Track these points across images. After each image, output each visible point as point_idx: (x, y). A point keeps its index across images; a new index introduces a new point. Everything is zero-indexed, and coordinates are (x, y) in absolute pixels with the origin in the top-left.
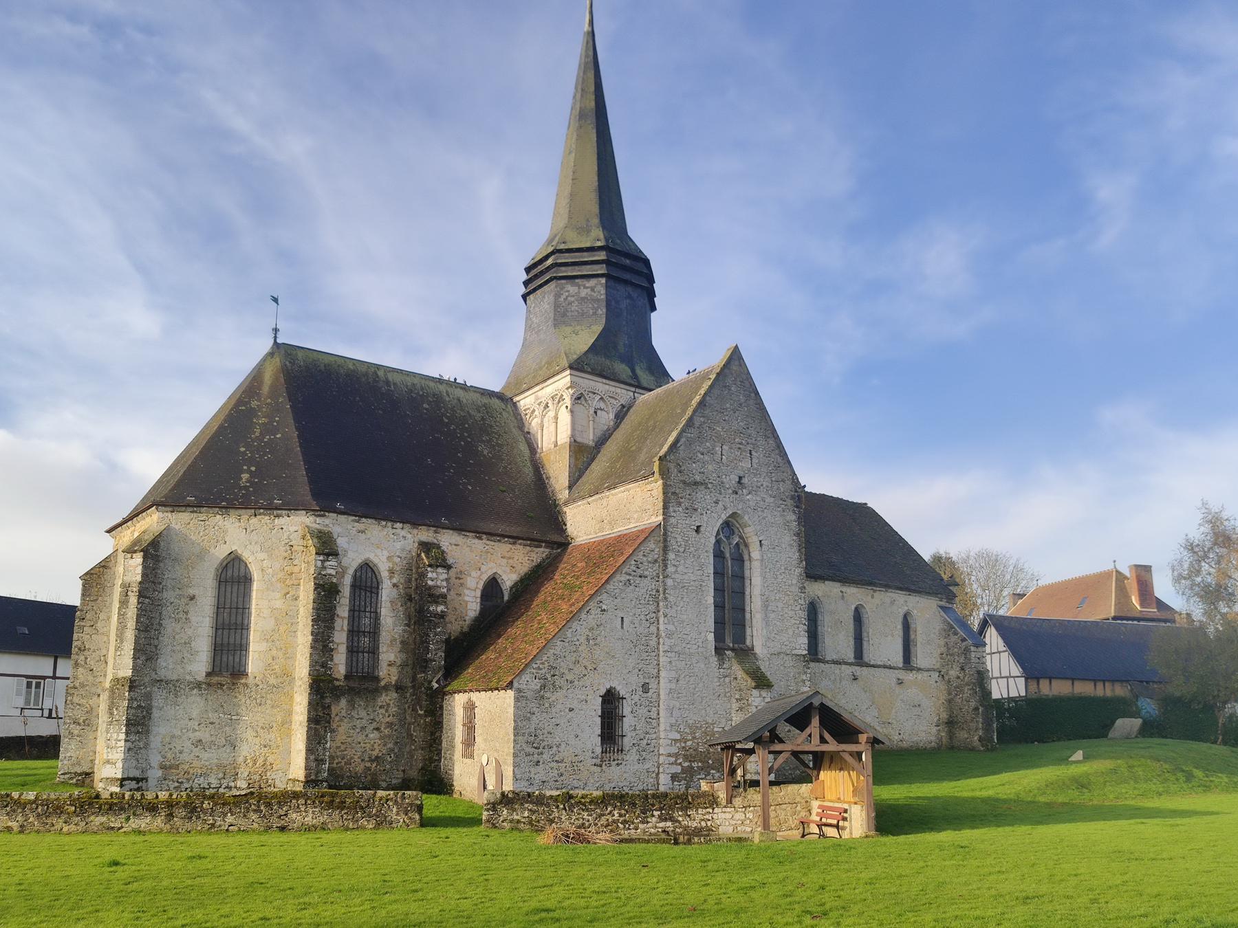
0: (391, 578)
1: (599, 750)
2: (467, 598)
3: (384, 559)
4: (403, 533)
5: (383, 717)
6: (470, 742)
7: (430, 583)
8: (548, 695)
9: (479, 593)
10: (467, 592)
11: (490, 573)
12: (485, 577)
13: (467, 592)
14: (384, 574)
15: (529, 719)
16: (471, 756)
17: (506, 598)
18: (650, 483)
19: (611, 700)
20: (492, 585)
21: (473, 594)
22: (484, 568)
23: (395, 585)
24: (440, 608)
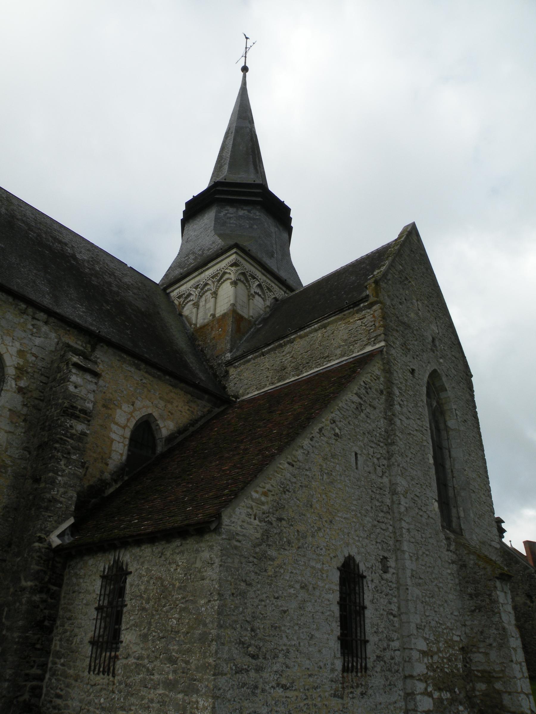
0: (17, 378)
1: (339, 664)
2: (113, 436)
3: (13, 350)
4: (45, 329)
5: (472, 655)
6: (108, 640)
7: (71, 388)
8: (272, 553)
9: (128, 434)
10: (114, 427)
11: (144, 412)
12: (138, 415)
13: (114, 427)
14: (11, 371)
15: (243, 594)
16: (108, 669)
17: (159, 449)
18: (361, 310)
19: (350, 576)
20: (144, 429)
21: (121, 432)
22: (138, 404)
23: (20, 390)
24: (80, 427)
